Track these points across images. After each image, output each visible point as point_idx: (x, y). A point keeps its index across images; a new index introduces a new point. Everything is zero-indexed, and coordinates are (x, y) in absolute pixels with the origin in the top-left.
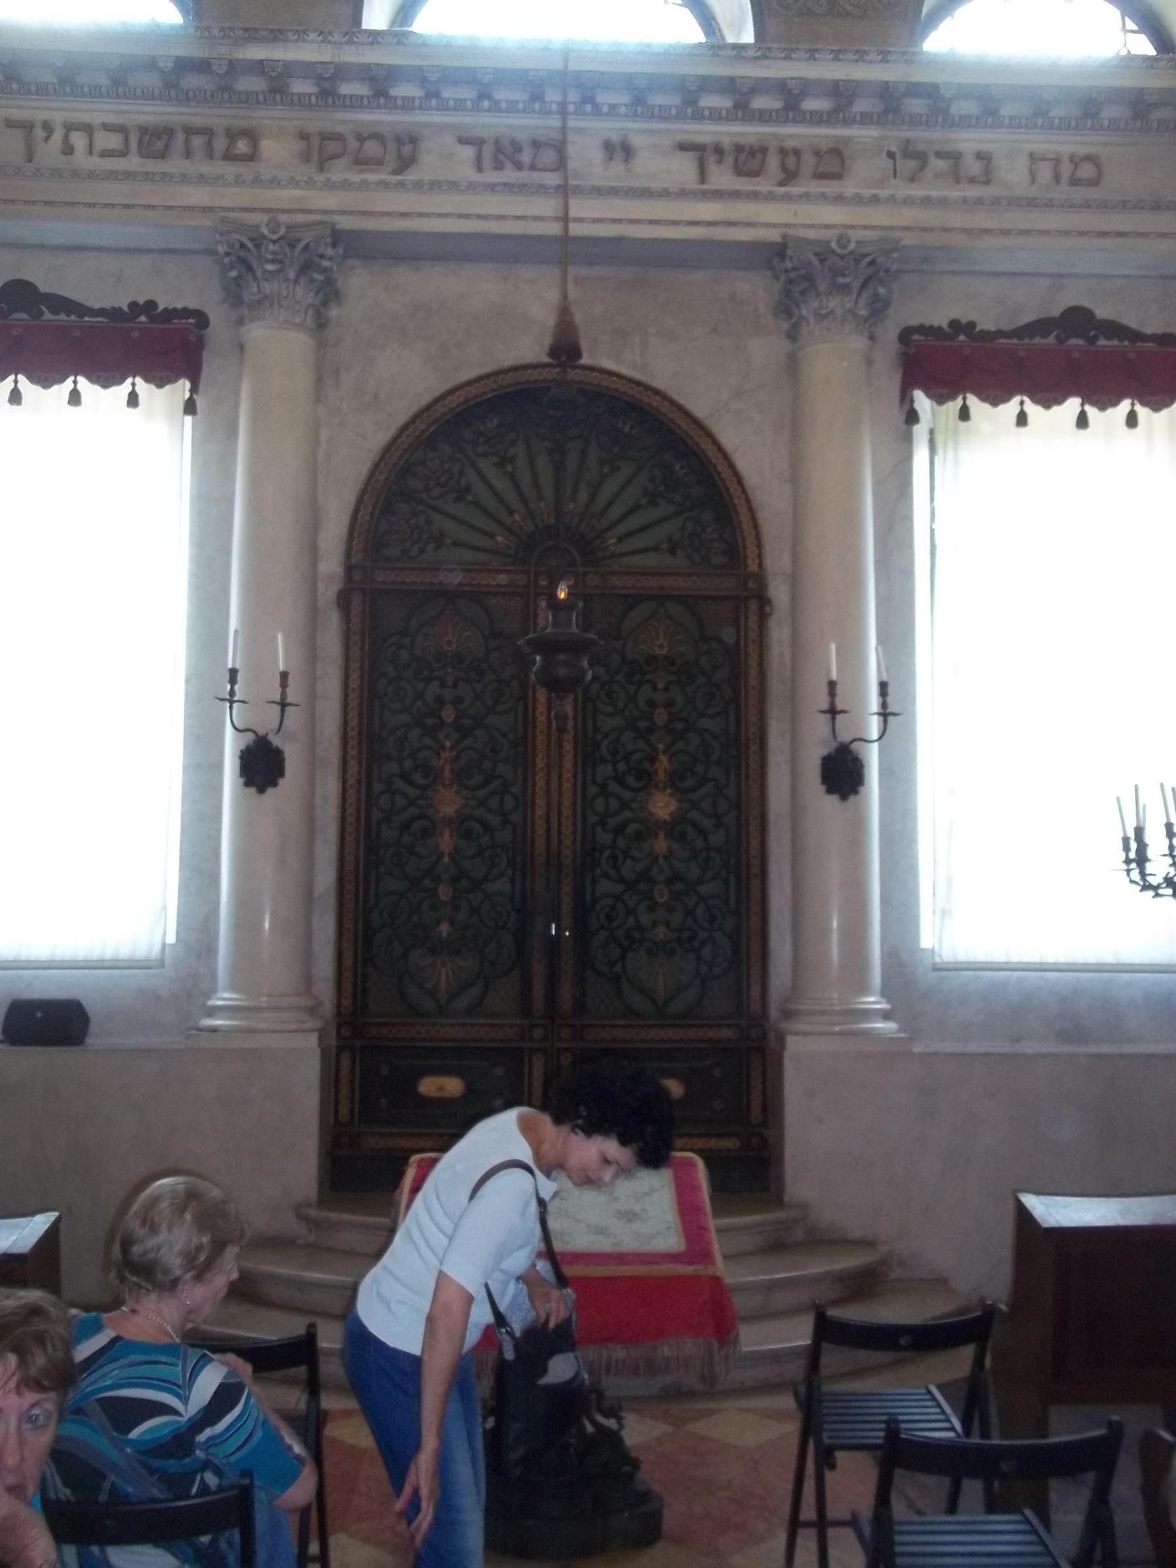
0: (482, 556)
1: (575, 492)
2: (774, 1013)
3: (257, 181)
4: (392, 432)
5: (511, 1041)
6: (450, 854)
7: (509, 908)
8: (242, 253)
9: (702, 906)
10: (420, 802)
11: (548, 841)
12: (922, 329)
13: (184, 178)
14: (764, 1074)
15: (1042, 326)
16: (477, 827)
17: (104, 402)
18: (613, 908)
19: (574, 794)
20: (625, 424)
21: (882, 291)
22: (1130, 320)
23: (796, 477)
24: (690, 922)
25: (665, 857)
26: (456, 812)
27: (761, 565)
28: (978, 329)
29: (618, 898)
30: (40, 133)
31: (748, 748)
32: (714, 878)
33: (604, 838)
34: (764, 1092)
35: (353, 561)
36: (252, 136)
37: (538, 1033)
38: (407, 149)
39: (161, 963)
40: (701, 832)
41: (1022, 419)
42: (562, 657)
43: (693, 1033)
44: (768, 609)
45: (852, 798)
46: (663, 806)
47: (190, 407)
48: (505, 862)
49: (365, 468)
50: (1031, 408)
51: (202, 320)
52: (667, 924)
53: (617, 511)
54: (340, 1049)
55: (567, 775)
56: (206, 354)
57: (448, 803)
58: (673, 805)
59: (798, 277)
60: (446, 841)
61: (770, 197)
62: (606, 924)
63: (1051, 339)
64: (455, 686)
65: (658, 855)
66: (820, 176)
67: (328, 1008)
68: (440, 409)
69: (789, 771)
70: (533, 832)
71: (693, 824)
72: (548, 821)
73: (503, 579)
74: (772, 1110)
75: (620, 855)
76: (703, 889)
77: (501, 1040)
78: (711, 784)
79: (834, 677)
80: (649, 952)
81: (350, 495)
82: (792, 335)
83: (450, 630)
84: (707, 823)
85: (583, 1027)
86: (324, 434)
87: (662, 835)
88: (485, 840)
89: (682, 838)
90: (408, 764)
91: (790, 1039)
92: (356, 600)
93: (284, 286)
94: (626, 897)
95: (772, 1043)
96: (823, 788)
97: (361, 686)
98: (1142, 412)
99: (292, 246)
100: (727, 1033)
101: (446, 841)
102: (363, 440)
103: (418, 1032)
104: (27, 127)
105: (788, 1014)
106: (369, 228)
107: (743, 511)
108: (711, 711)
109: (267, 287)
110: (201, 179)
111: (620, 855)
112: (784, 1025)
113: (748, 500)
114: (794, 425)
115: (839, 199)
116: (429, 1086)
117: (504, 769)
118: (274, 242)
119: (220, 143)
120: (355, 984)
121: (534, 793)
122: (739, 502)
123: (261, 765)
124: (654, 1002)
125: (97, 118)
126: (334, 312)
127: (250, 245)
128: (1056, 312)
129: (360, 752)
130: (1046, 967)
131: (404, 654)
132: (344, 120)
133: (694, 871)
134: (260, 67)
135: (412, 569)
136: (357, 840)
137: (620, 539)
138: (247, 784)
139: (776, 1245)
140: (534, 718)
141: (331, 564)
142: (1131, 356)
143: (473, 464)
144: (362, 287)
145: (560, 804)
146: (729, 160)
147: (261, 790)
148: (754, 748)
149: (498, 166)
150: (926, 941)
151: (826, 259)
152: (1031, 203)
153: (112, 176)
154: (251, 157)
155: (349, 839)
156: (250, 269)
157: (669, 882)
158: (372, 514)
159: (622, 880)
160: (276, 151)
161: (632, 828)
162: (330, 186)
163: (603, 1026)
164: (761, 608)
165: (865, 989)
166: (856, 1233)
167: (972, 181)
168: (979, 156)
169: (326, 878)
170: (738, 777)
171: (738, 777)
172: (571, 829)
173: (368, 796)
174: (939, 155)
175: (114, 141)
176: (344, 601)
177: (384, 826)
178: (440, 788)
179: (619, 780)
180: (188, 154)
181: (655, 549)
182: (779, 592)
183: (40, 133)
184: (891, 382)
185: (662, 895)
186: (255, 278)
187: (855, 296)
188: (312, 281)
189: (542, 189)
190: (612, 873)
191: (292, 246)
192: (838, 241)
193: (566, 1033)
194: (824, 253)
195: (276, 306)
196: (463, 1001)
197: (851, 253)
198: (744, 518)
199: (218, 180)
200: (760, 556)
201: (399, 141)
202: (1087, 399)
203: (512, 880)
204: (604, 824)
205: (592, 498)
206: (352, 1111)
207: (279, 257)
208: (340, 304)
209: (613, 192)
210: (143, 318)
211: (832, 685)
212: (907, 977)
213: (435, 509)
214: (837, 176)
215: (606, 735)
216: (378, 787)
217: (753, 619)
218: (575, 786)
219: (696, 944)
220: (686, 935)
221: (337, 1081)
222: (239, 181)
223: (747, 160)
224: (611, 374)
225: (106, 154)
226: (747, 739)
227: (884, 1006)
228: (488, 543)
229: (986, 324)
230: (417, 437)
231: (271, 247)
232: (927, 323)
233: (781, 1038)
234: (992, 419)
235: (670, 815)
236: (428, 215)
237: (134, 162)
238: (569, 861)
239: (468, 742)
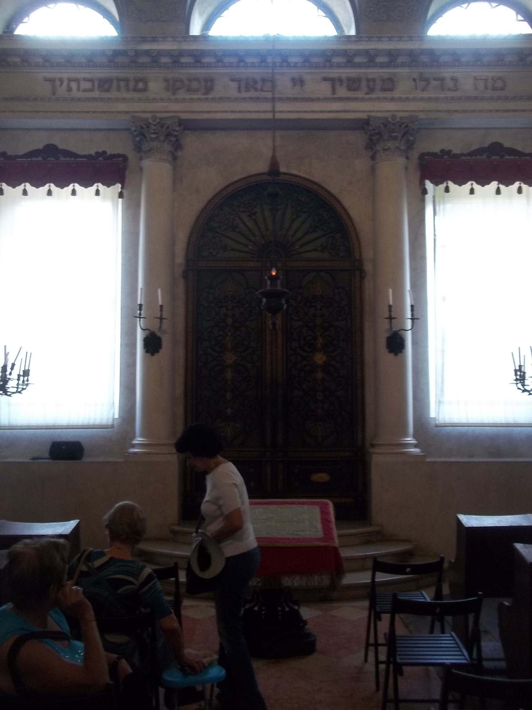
3: (147, 100)
4: (204, 203)
12: (429, 154)
13: (117, 100)
21: (411, 138)
22: (519, 148)
27: (360, 256)
30: (58, 83)
36: (144, 80)
38: (209, 84)
39: (112, 426)
41: (472, 192)
45: (400, 355)
46: (320, 358)
47: (121, 195)
50: (476, 187)
56: (127, 173)
57: (230, 358)
58: (324, 358)
60: (229, 374)
61: (363, 99)
63: (484, 157)
66: (384, 90)
79: (391, 303)
82: (373, 158)
96: (387, 350)
99: (162, 127)
101: (229, 374)
102: (194, 206)
104: (52, 81)
105: (373, 446)
109: (154, 144)
110: (124, 100)
112: (371, 450)
115: (392, 99)
118: (155, 125)
119: (132, 85)
123: (152, 344)
125: (81, 76)
126: (179, 153)
128: (486, 144)
130: (447, 425)
132: (183, 73)
134: (147, 53)
137: (301, 246)
141: (180, 259)
144: (192, 143)
146: (345, 84)
147: (153, 354)
149: (247, 90)
150: (433, 414)
152: (476, 98)
153: (88, 100)
154: (145, 90)
156: (145, 136)
160: (155, 87)
162: (177, 101)
167: (449, 90)
168: (452, 79)
174: (435, 79)
175: (88, 85)
176: (185, 276)
180: (119, 89)
182: (368, 267)
183: (58, 83)
184: (416, 176)
188: (171, 141)
189: (266, 99)
191: (162, 127)
194: (386, 123)
197: (398, 122)
199: (132, 100)
201: (206, 81)
202: (501, 182)
207: (157, 131)
209: (295, 99)
210: (101, 158)
212: (426, 431)
214: (391, 90)
222: (140, 100)
223: (353, 84)
225: (85, 90)
227: (414, 442)
229: (456, 151)
231: (153, 127)
235: (323, 362)
237: (96, 94)
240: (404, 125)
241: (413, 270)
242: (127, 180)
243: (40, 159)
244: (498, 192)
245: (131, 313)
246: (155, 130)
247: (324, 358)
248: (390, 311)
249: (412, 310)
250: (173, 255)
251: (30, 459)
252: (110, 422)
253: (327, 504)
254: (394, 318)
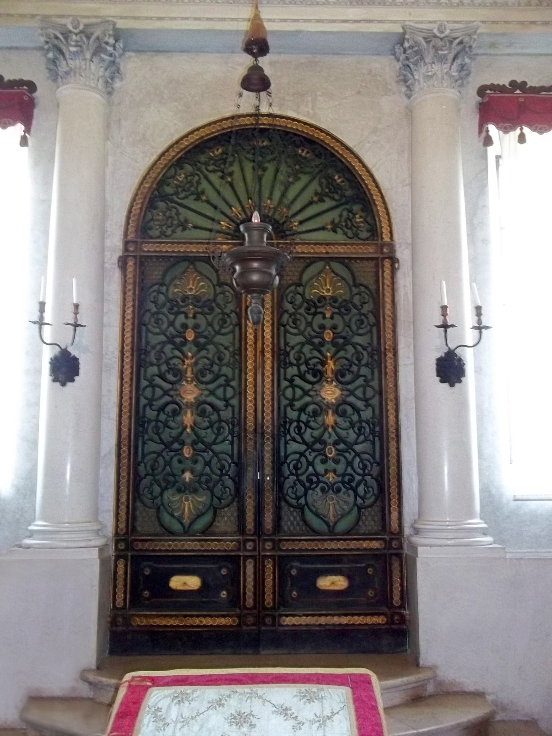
1: (271, 194)
2: (407, 531)
4: (154, 157)
5: (232, 551)
6: (191, 426)
7: (230, 462)
8: (56, 42)
10: (172, 393)
11: (256, 417)
12: (493, 87)
14: (401, 571)
16: (209, 408)
18: (298, 461)
19: (273, 386)
20: (303, 151)
24: (349, 470)
25: (333, 427)
26: (195, 398)
27: (391, 237)
28: (528, 86)
29: (302, 454)
31: (385, 355)
32: (366, 440)
33: (292, 414)
34: (402, 585)
35: (129, 238)
37: (250, 546)
40: (356, 410)
42: (255, 265)
43: (353, 545)
44: (396, 265)
45: (457, 385)
48: (227, 432)
49: (136, 181)
51: (32, 86)
52: (335, 471)
53: (297, 206)
54: (117, 558)
55: (268, 373)
56: (36, 112)
57: (190, 393)
58: (338, 392)
60: (188, 418)
62: (294, 471)
65: (328, 426)
69: (414, 369)
70: (246, 411)
71: (350, 404)
72: (255, 405)
74: (408, 596)
75: (303, 425)
76: (358, 448)
77: (225, 551)
78: (362, 379)
80: (323, 490)
81: (127, 198)
83: (191, 282)
84: (360, 404)
85: (281, 540)
86: (110, 159)
87: (330, 412)
88: (214, 417)
89: (343, 414)
90: (164, 368)
91: (420, 549)
92: (131, 263)
93: (83, 62)
94: (307, 454)
95: (406, 550)
97: (133, 318)
99: (88, 38)
100: (375, 545)
101: (188, 418)
103: (170, 546)
105: (417, 531)
106: (137, 27)
107: (379, 203)
111: (303, 425)
112: (416, 539)
114: (411, 149)
116: (177, 582)
117: (226, 370)
118: (76, 34)
120: (127, 513)
121: (246, 386)
122: (377, 198)
123: (65, 368)
124: (327, 523)
126: (117, 84)
127: (60, 36)
129: (132, 360)
131: (162, 298)
135: (167, 243)
136: (130, 417)
137: (301, 223)
138: (55, 380)
139: (417, 699)
140: (246, 337)
143: (206, 178)
145: (263, 393)
147: (63, 384)
148: (390, 355)
151: (430, 41)
155: (125, 417)
157: (335, 443)
158: (141, 209)
161: (311, 408)
163: (294, 540)
164: (392, 265)
165: (471, 515)
166: (471, 688)
170: (380, 372)
171: (380, 372)
172: (270, 409)
176: (123, 263)
177: (148, 408)
178: (184, 383)
179: (302, 377)
182: (403, 254)
185: (331, 452)
186: (65, 59)
187: (449, 65)
188: (103, 60)
190: (156, 437)
191: (88, 38)
192: (439, 29)
193: (268, 545)
195: (78, 75)
196: (199, 525)
197: (447, 36)
203: (232, 443)
204: (291, 405)
205: (283, 195)
206: (125, 599)
207: (79, 44)
208: (122, 79)
211: (444, 308)
213: (181, 205)
215: (293, 348)
216: (144, 383)
217: (387, 272)
218: (273, 380)
219: (354, 484)
220: (347, 478)
221: (115, 579)
224: (293, 120)
226: (385, 349)
229: (532, 82)
230: (170, 160)
231: (74, 37)
232: (496, 83)
233: (414, 548)
235: (336, 399)
236: (175, 19)
238: (269, 430)
239: (204, 353)
240: (457, 41)
241: (473, 260)
242: (34, 122)
246: (76, 41)
247: (338, 392)
248: (444, 315)
250: (103, 234)
251: (485, 490)
253: (367, 681)
254: (453, 326)
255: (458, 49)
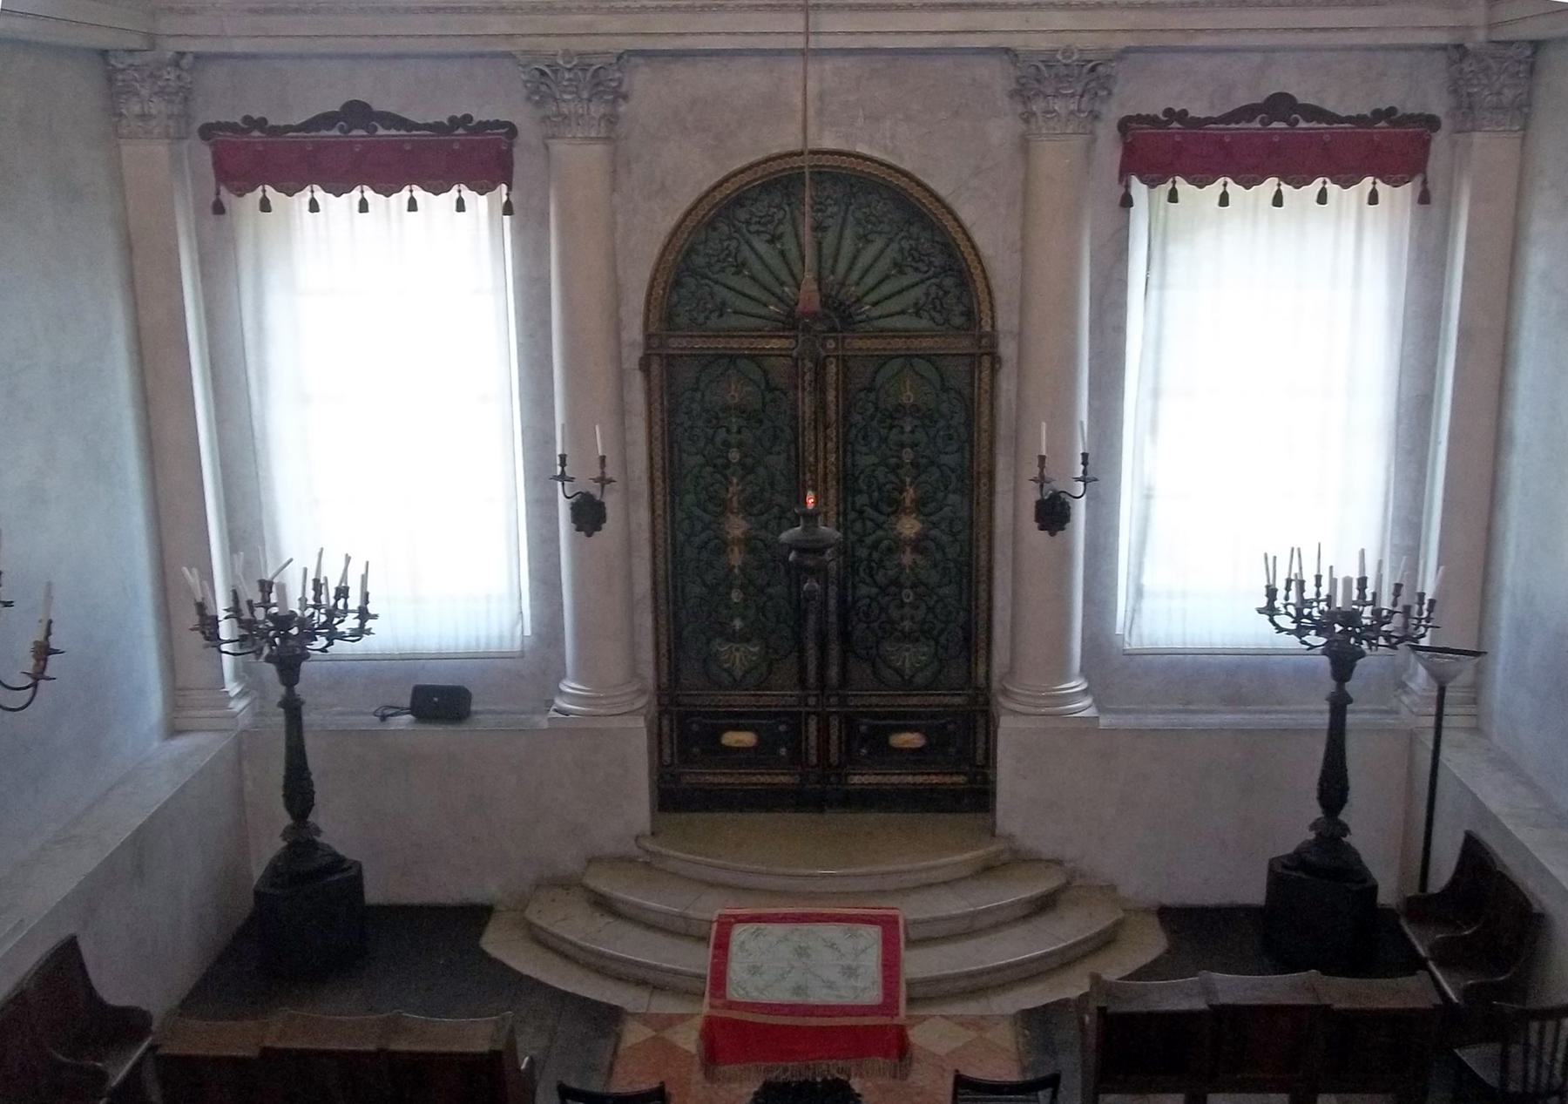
0: (759, 322)
9: (940, 605)
12: (1139, 118)
15: (1248, 112)
16: (760, 545)
17: (437, 205)
22: (1330, 105)
23: (1024, 247)
24: (930, 616)
27: (993, 326)
33: (863, 553)
39: (522, 655)
40: (940, 547)
46: (909, 527)
47: (508, 209)
50: (1234, 189)
52: (912, 618)
54: (661, 714)
57: (737, 527)
58: (918, 526)
59: (1036, 79)
60: (736, 558)
63: (1256, 124)
64: (739, 432)
67: (650, 683)
68: (718, 196)
69: (1013, 505)
73: (775, 344)
76: (941, 591)
82: (1027, 117)
86: (620, 219)
92: (655, 368)
96: (1036, 525)
98: (1333, 189)
101: (736, 558)
102: (652, 226)
108: (949, 449)
112: (1001, 699)
113: (983, 271)
116: (731, 738)
118: (570, 70)
123: (588, 515)
133: (934, 577)
137: (875, 304)
141: (634, 332)
142: (1327, 138)
144: (640, 80)
159: (875, 584)
164: (993, 365)
165: (1066, 678)
169: (643, 584)
173: (673, 522)
181: (903, 312)
182: (1007, 349)
184: (1109, 152)
190: (868, 580)
193: (833, 700)
198: (980, 285)
200: (993, 318)
204: (861, 541)
210: (460, 131)
212: (1112, 666)
216: (680, 515)
217: (986, 374)
228: (762, 311)
229: (1198, 110)
231: (567, 76)
234: (1197, 199)
243: (335, 132)
244: (1278, 201)
245: (545, 471)
247: (918, 526)
249: (1085, 463)
250: (617, 327)
252: (517, 647)
255: (1093, 74)
